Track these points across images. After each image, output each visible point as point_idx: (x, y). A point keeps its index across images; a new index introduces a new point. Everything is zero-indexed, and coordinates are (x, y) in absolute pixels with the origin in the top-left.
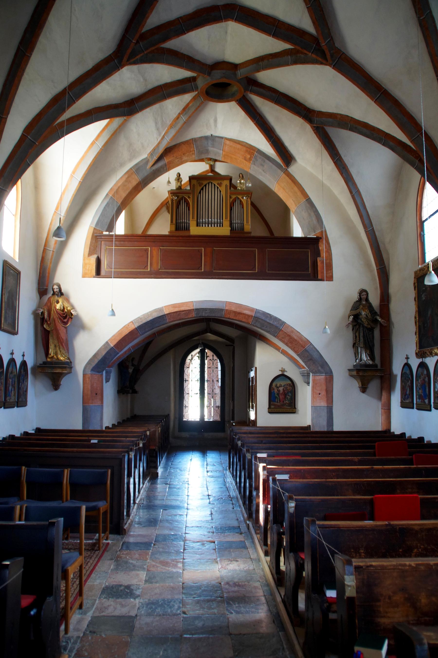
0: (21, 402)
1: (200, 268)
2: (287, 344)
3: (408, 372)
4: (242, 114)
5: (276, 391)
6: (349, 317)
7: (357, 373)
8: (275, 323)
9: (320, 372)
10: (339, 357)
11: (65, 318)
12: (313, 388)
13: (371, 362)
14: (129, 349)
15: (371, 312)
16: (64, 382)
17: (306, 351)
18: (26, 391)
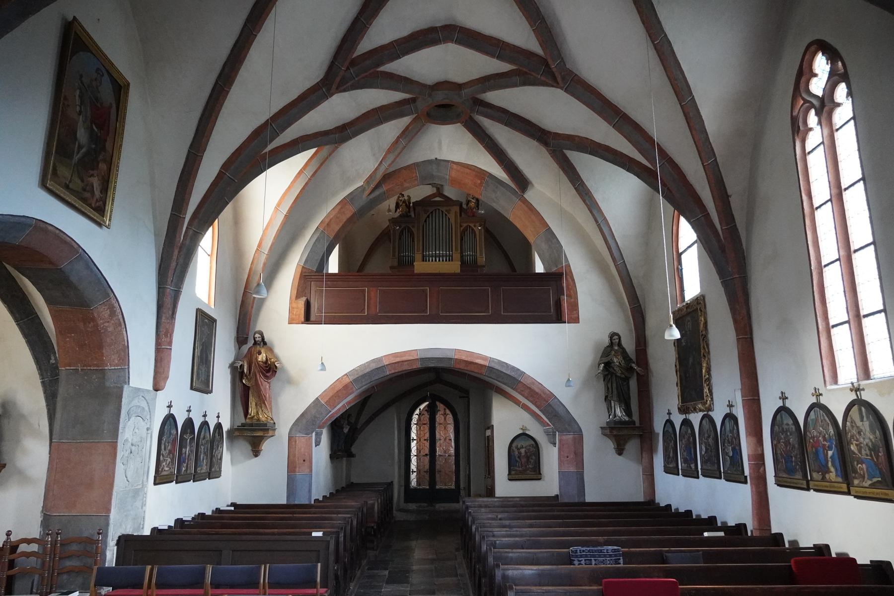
0: (213, 473)
1: (425, 311)
2: (526, 398)
3: (670, 430)
4: (469, 137)
5: (516, 453)
6: (599, 365)
8: (512, 374)
10: (588, 411)
11: (268, 371)
12: (560, 449)
13: (627, 419)
14: (344, 406)
16: (266, 446)
17: (550, 405)
18: (221, 459)
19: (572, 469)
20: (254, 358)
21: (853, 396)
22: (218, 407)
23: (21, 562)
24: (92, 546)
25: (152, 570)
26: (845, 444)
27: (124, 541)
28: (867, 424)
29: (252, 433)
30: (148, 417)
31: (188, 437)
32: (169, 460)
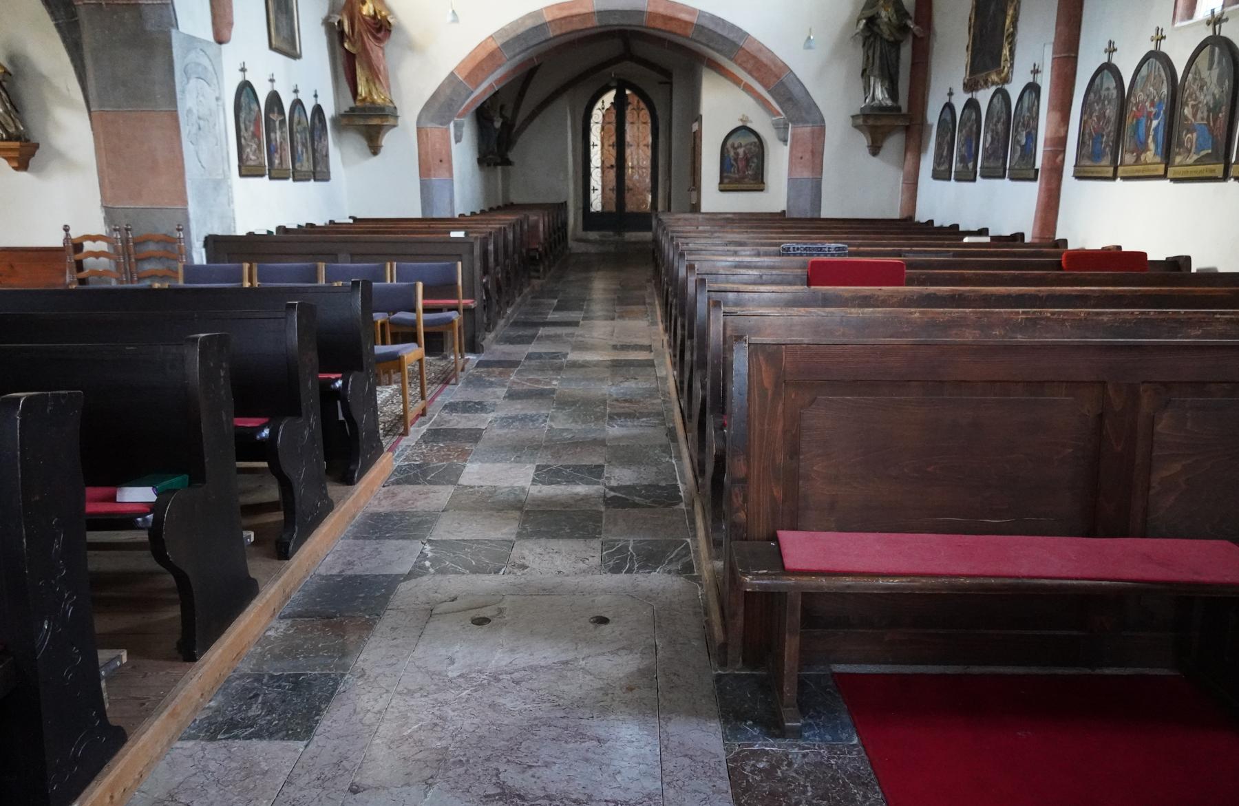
0: (319, 173)
2: (750, 73)
3: (949, 118)
5: (732, 154)
7: (865, 121)
8: (731, 36)
9: (805, 121)
10: (836, 92)
11: (379, 30)
13: (889, 103)
14: (491, 86)
15: (897, 11)
16: (388, 140)
17: (782, 83)
18: (327, 155)
19: (807, 174)
20: (356, 12)
21: (1209, 32)
22: (309, 79)
23: (89, 262)
24: (173, 246)
25: (250, 269)
26: (1178, 105)
27: (213, 243)
28: (1215, 72)
29: (368, 123)
30: (215, 81)
31: (275, 116)
32: (254, 146)
